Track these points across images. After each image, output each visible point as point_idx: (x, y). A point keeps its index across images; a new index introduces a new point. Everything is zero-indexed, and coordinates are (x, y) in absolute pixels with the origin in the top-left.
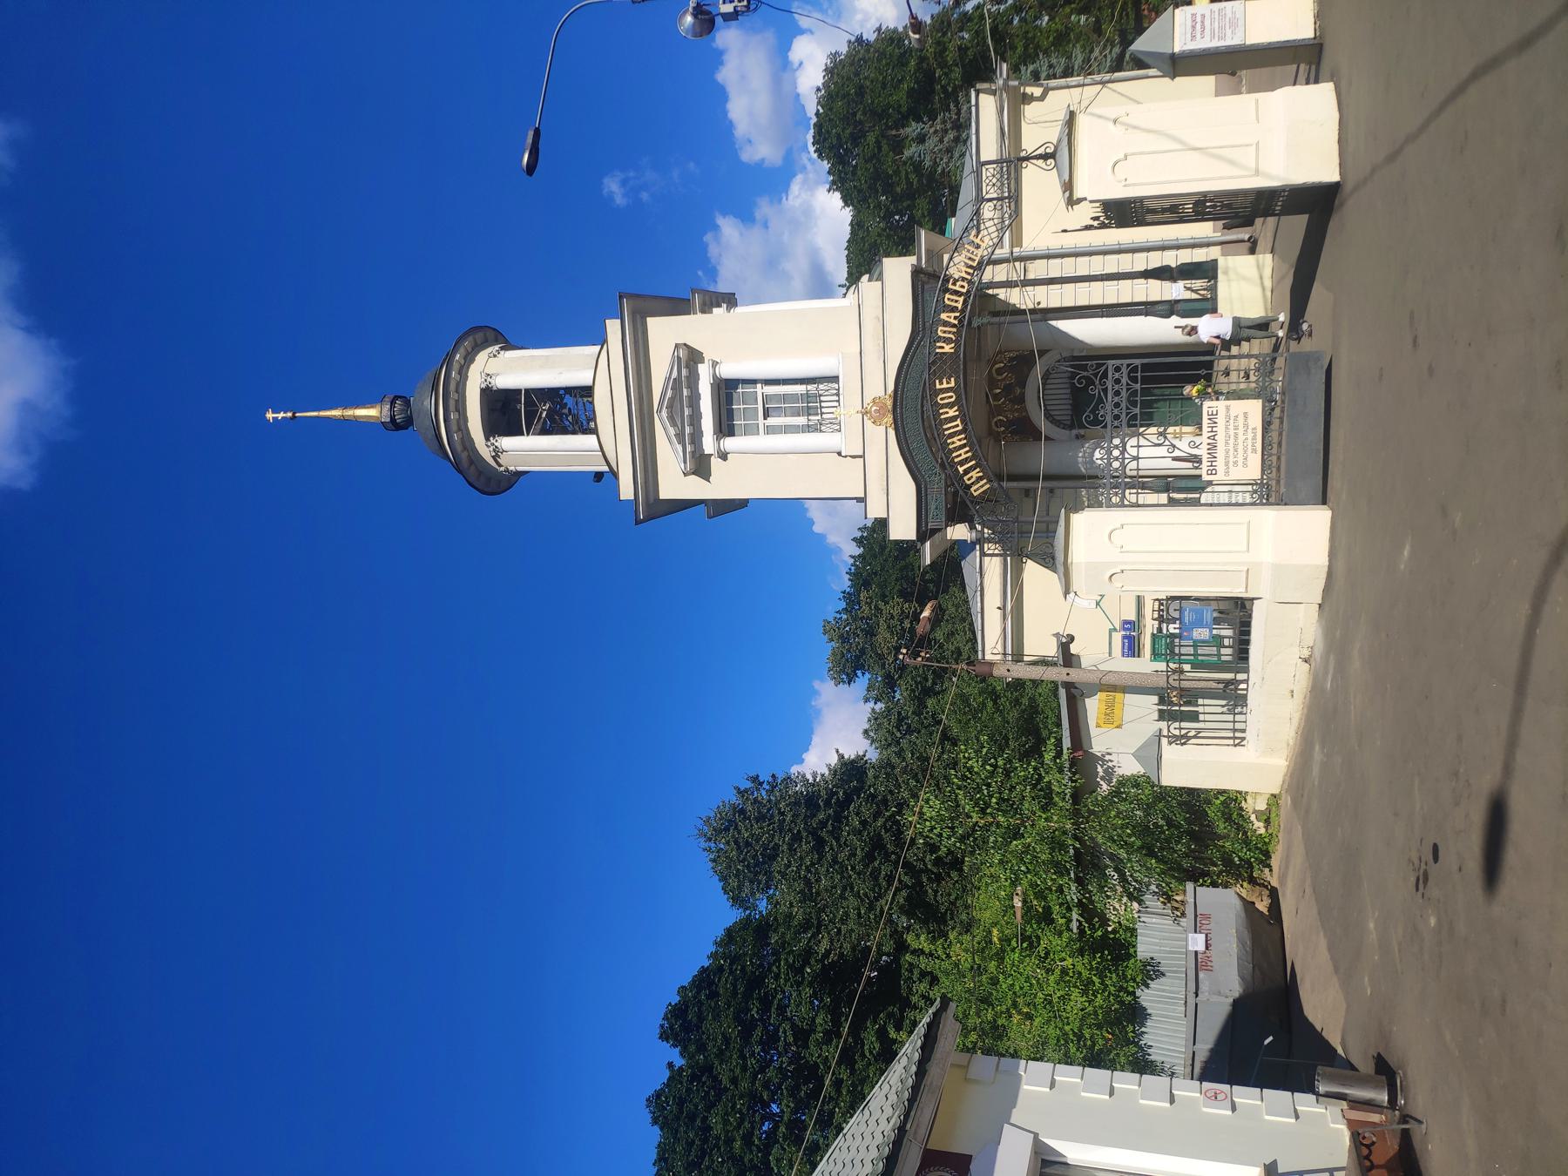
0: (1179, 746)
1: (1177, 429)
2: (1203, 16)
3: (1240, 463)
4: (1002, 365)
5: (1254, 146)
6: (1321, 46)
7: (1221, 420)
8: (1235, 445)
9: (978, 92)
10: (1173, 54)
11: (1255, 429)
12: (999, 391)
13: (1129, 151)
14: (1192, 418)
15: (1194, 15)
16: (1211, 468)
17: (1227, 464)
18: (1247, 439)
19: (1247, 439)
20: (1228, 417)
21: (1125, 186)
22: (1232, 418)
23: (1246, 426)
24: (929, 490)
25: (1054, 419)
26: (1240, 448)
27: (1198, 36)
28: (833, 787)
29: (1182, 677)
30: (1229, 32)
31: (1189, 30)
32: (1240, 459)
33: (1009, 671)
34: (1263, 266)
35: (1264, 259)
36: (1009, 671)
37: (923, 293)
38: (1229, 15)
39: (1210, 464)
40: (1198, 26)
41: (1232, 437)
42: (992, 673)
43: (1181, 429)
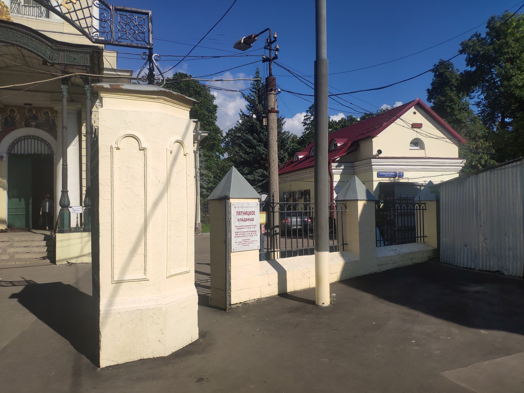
2: (252, 220)
4: (50, 115)
5: (144, 277)
6: (225, 310)
9: (196, 122)
10: (229, 199)
12: (34, 113)
13: (149, 153)
15: (253, 213)
21: (111, 147)
25: (15, 144)
27: (240, 217)
30: (240, 239)
31: (244, 210)
38: (252, 239)
40: (246, 217)
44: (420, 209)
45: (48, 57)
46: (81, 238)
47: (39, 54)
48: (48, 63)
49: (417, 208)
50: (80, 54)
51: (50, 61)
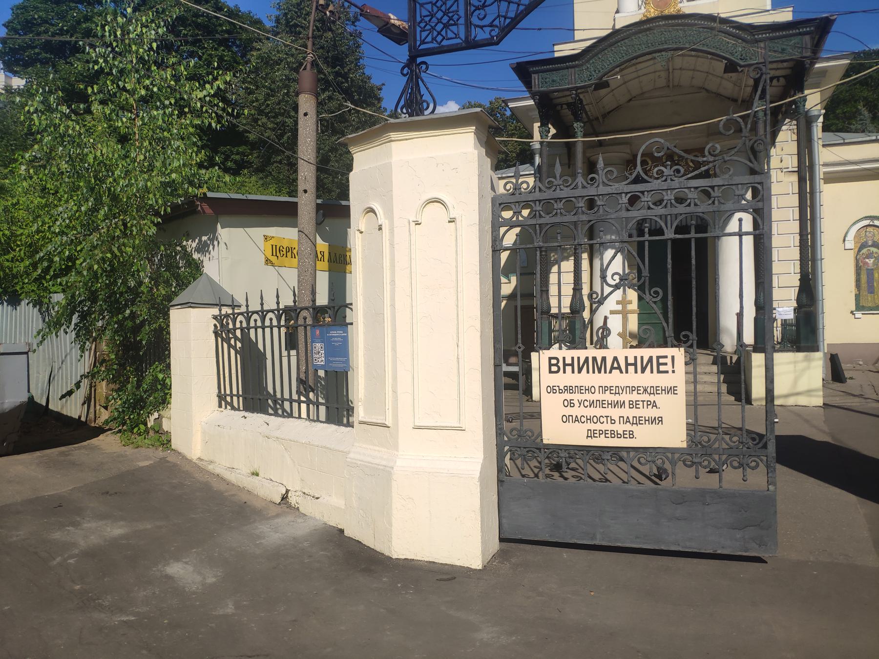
0: (213, 328)
1: (634, 306)
3: (569, 411)
7: (649, 379)
8: (602, 404)
11: (631, 435)
14: (75, 524)
16: (561, 364)
17: (569, 389)
18: (613, 422)
19: (613, 422)
20: (655, 390)
22: (652, 398)
23: (638, 421)
24: (573, 70)
26: (598, 412)
28: (351, 78)
29: (308, 328)
32: (576, 411)
33: (306, 114)
34: (811, 396)
35: (818, 396)
36: (306, 114)
37: (800, 34)
39: (568, 361)
41: (616, 398)
42: (301, 93)
43: (632, 312)
44: (263, 328)
45: (739, 57)
46: (795, 362)
47: (724, 55)
48: (738, 68)
49: (271, 323)
50: (792, 38)
51: (742, 63)
